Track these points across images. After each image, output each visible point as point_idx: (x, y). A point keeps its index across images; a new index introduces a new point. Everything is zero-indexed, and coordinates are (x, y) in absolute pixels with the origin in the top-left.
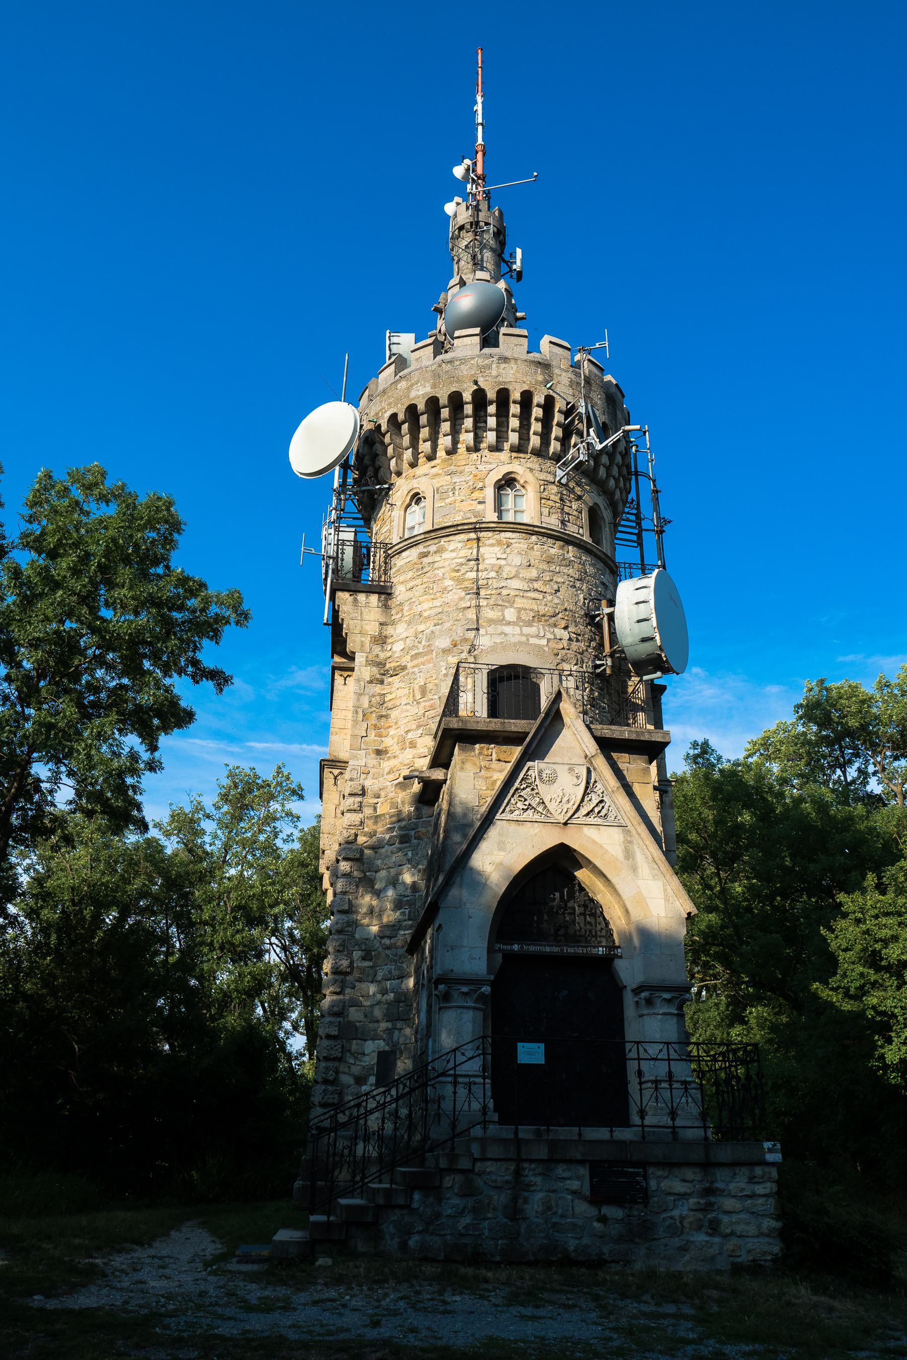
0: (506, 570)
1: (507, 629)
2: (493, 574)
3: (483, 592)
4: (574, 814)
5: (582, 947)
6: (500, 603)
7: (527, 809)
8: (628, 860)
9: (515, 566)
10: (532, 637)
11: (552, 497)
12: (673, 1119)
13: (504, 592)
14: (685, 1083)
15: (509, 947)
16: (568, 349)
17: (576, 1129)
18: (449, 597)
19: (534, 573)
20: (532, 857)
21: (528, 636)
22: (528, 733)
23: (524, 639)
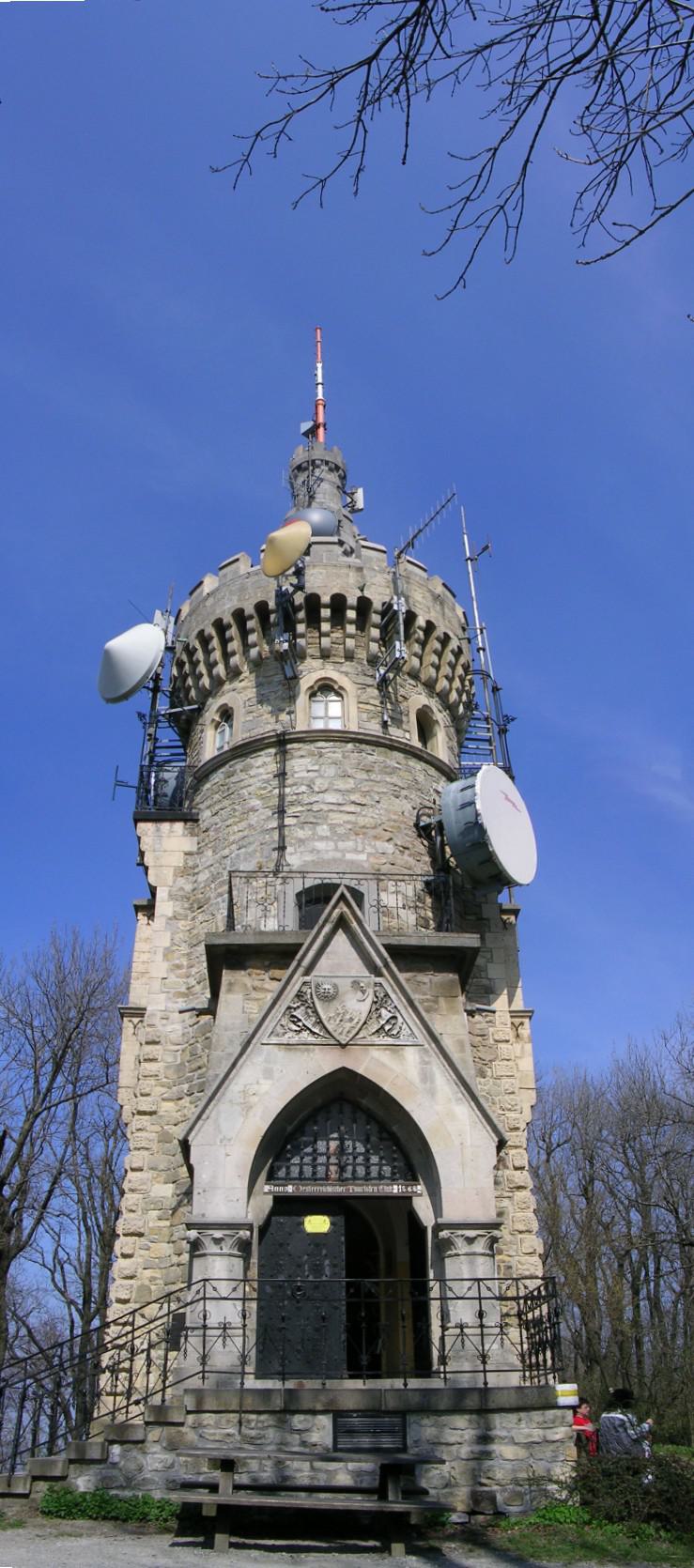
0: (318, 782)
1: (320, 845)
2: (303, 788)
3: (290, 811)
4: (357, 1034)
5: (373, 1185)
6: (312, 820)
7: (300, 1031)
8: (425, 1083)
9: (328, 777)
10: (349, 852)
11: (372, 701)
12: (484, 1362)
13: (315, 808)
14: (461, 1327)
15: (281, 1189)
16: (384, 552)
17: (320, 1381)
18: (253, 819)
19: (350, 784)
20: (305, 1085)
21: (344, 851)
22: (301, 945)
23: (338, 855)
